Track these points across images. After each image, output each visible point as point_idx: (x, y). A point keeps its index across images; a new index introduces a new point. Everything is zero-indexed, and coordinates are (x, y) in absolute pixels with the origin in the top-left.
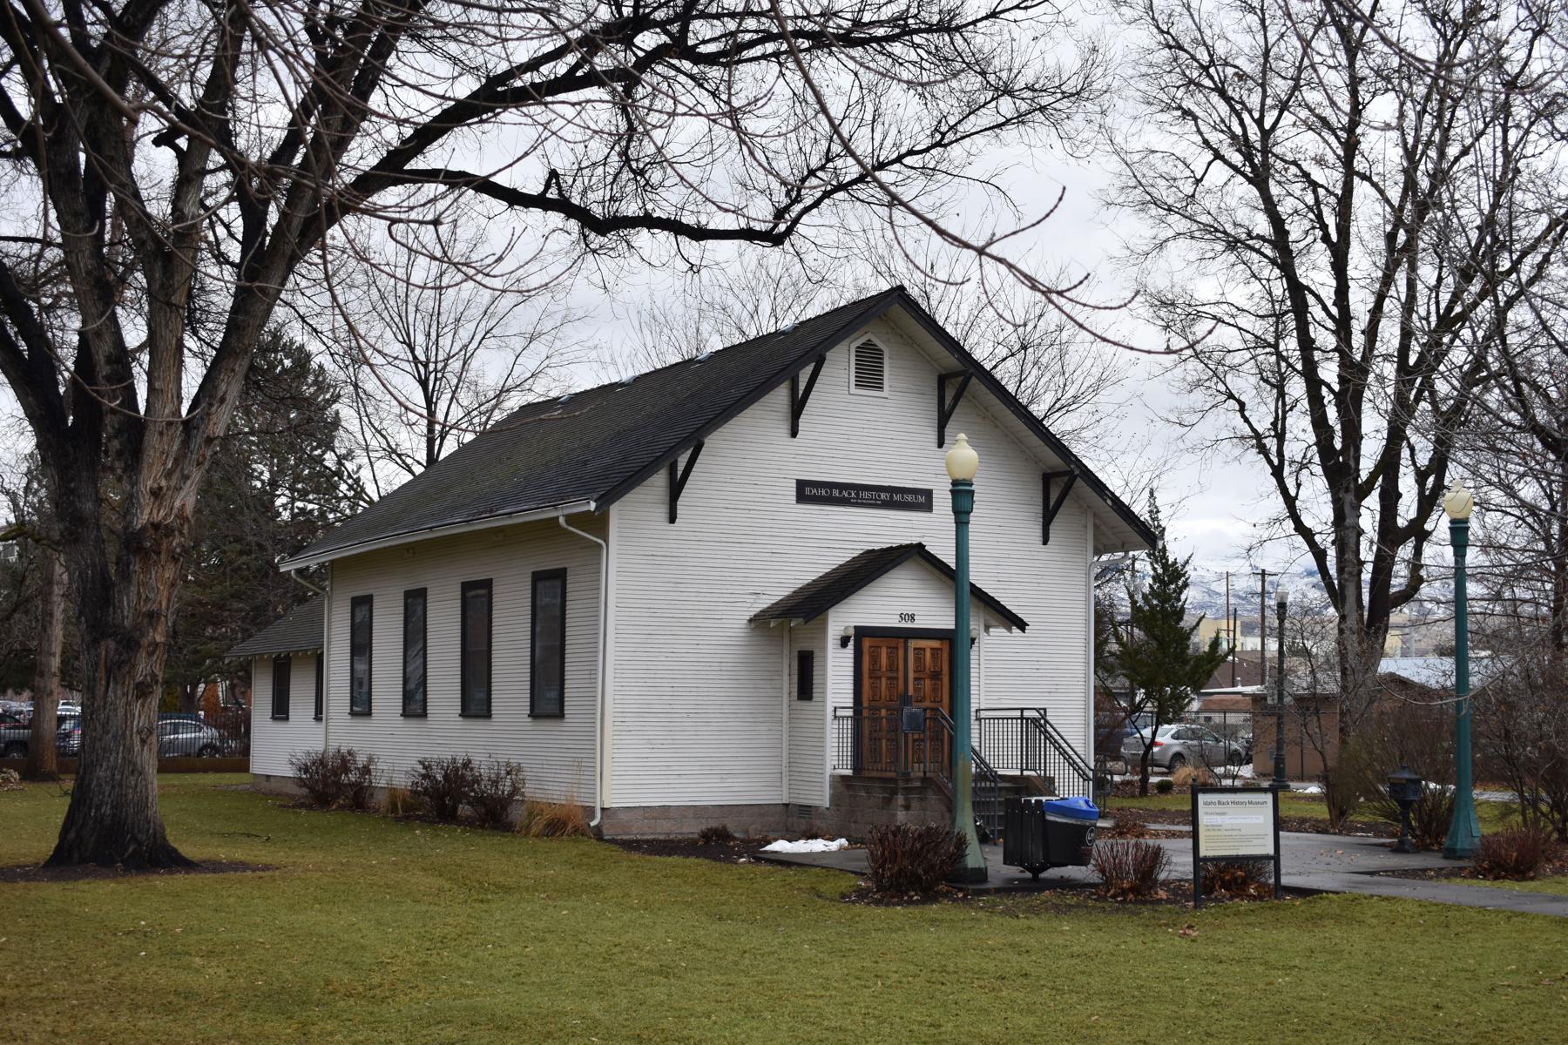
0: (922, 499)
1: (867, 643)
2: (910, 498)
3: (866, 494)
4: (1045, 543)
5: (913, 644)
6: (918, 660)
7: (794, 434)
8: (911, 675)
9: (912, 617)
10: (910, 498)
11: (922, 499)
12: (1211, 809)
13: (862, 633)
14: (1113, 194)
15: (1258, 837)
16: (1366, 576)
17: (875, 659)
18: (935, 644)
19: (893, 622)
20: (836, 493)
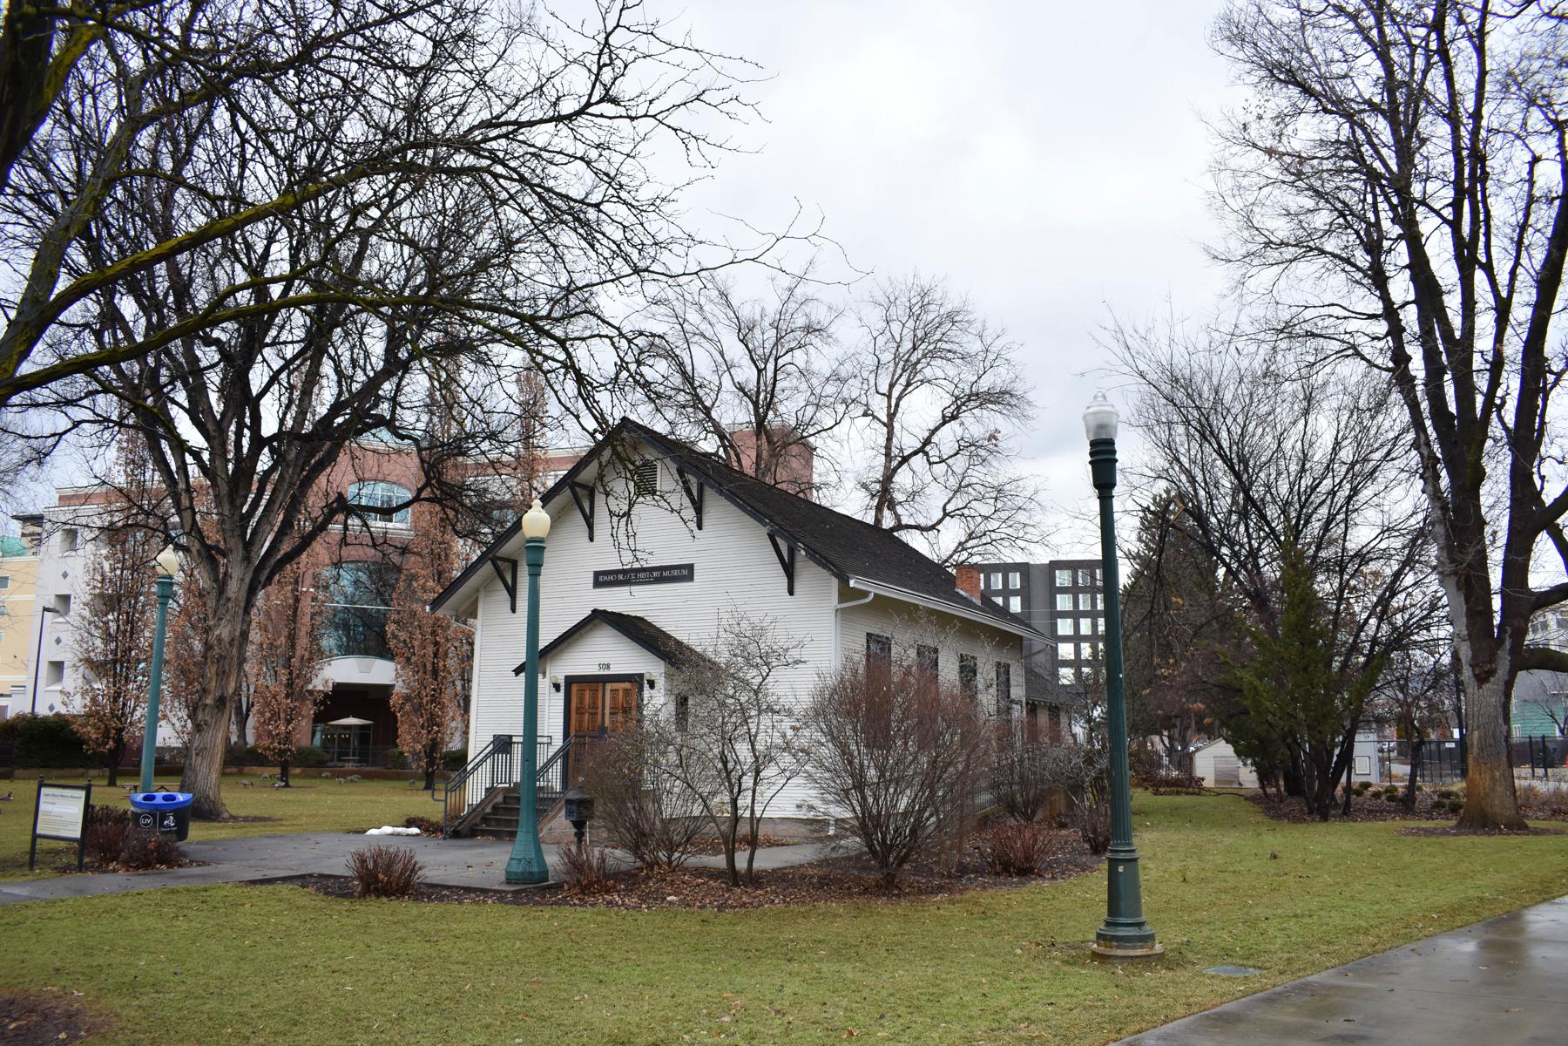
0: (685, 572)
1: (575, 688)
2: (675, 573)
3: (642, 575)
4: (791, 592)
5: (609, 686)
6: (614, 699)
7: (591, 539)
8: (607, 711)
9: (608, 666)
10: (675, 573)
11: (685, 572)
12: (51, 799)
13: (570, 680)
14: (1225, 292)
15: (71, 823)
16: (1496, 578)
17: (581, 699)
18: (627, 685)
19: (593, 670)
20: (621, 577)
